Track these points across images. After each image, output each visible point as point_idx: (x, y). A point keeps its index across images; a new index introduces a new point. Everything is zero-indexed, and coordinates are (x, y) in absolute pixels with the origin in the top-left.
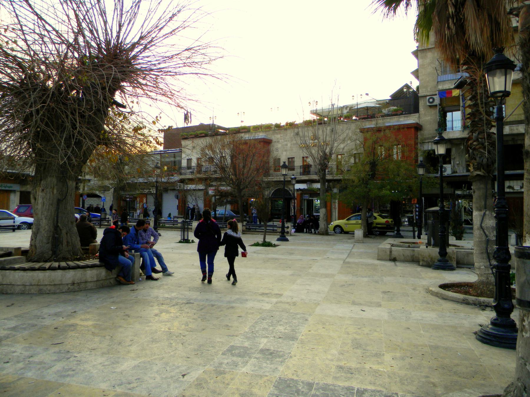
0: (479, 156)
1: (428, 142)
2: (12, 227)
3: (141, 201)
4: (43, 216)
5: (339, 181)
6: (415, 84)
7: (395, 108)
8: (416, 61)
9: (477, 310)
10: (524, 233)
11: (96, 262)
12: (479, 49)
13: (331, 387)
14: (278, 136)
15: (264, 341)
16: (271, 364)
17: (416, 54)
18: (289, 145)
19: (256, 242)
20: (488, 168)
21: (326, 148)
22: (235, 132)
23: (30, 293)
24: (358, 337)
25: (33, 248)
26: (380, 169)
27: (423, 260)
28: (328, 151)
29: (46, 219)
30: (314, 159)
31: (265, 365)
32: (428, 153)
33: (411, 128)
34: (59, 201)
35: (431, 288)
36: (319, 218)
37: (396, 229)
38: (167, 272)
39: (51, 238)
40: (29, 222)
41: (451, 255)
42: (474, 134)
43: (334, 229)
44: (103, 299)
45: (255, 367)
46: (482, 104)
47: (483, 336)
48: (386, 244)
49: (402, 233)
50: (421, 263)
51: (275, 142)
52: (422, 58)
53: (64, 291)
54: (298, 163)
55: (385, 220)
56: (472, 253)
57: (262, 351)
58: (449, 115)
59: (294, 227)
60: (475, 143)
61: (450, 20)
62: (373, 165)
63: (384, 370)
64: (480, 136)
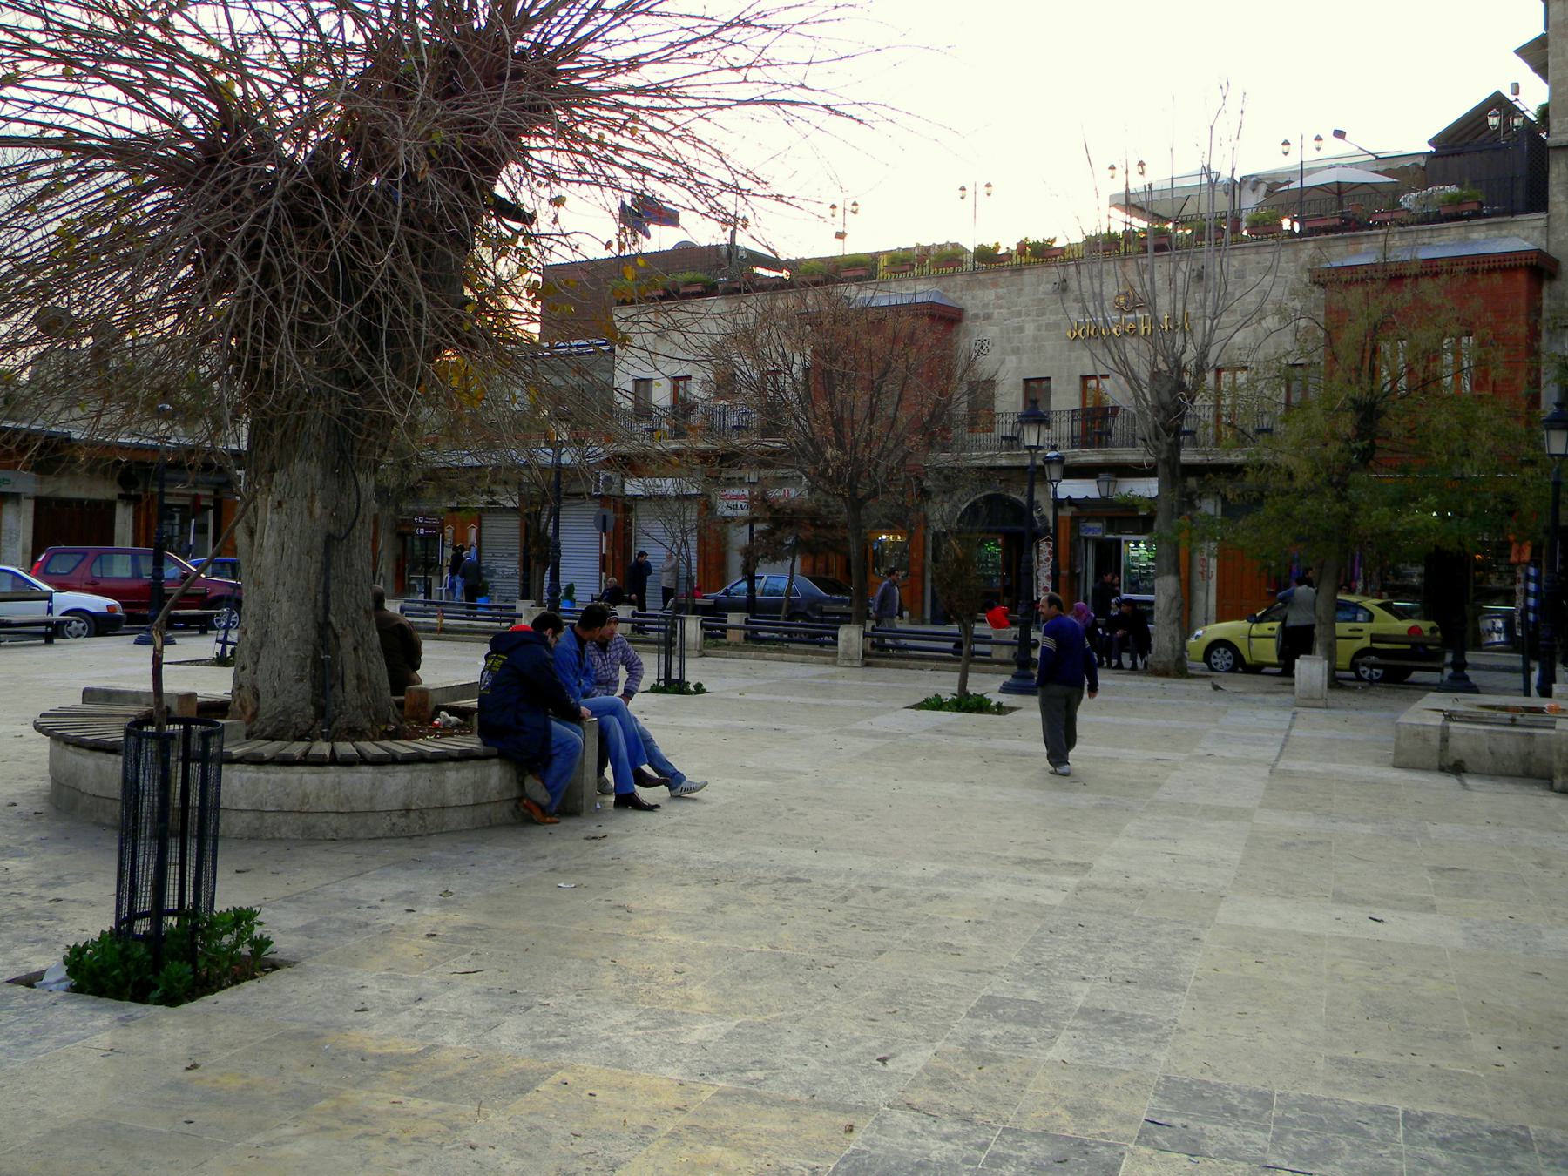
2: (43, 629)
5: (1233, 471)
6: (1533, 95)
7: (1453, 189)
11: (472, 743)
13: (1324, 1104)
14: (990, 295)
15: (1086, 988)
18: (1030, 329)
19: (931, 696)
21: (1184, 347)
22: (819, 278)
23: (278, 836)
24: (1375, 989)
25: (247, 695)
26: (1396, 431)
28: (1189, 357)
30: (1132, 379)
31: (1108, 1046)
33: (1515, 269)
34: (330, 540)
36: (1152, 612)
37: (1449, 658)
39: (308, 662)
40: (93, 610)
44: (516, 861)
45: (1082, 1050)
49: (1473, 676)
50: (1558, 782)
51: (976, 316)
53: (380, 833)
54: (1064, 399)
55: (1406, 624)
57: (1084, 1013)
62: (1368, 413)
63: (1478, 1073)
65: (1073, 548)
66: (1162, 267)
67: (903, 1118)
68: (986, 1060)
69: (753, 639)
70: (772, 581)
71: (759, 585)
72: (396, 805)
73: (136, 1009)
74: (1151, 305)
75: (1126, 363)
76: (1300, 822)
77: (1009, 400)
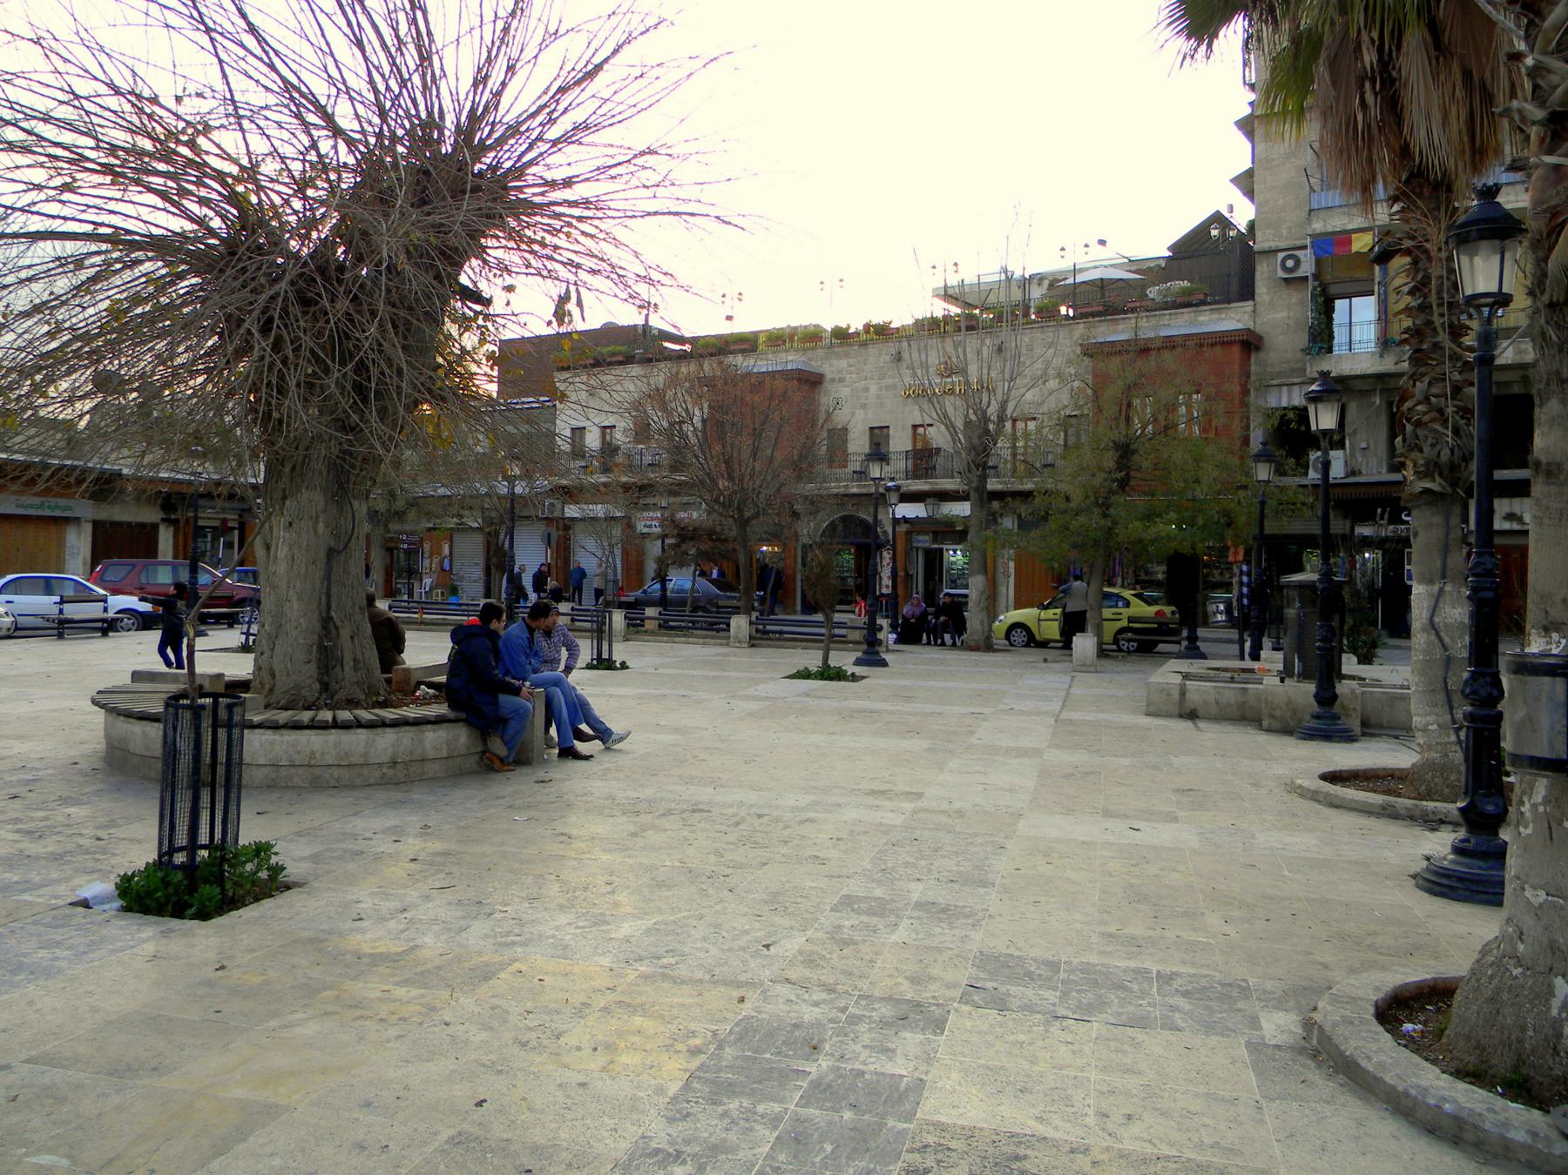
0: (1430, 441)
1: (1280, 385)
3: (436, 550)
4: (291, 592)
5: (1026, 495)
6: (1243, 213)
7: (1186, 284)
8: (1248, 146)
9: (1417, 831)
10: (1528, 627)
11: (441, 709)
12: (1436, 162)
14: (843, 363)
16: (952, 928)
17: (1247, 126)
18: (873, 389)
20: (1452, 473)
21: (989, 403)
22: (714, 351)
25: (265, 675)
26: (1145, 464)
27: (1272, 716)
28: (992, 411)
29: (299, 598)
30: (951, 427)
31: (937, 930)
32: (1282, 417)
33: (1230, 343)
34: (331, 553)
35: (1299, 782)
37: (1185, 633)
38: (613, 737)
41: (1346, 703)
42: (1418, 384)
43: (1008, 636)
46: (1440, 305)
47: (1433, 878)
48: (1168, 673)
50: (1265, 723)
51: (833, 380)
52: (1267, 138)
53: (372, 781)
54: (900, 442)
55: (1155, 609)
56: (1405, 699)
57: (919, 905)
58: (1340, 305)
59: (894, 627)
60: (1419, 408)
61: (1367, 85)
62: (1125, 451)
64: (1434, 391)
65: (907, 555)
66: (972, 342)
67: (783, 990)
68: (844, 943)
69: (665, 627)
70: (679, 583)
71: (670, 586)
72: (385, 758)
73: (175, 923)
74: (963, 371)
75: (946, 415)
76: (1079, 758)
77: (858, 444)
